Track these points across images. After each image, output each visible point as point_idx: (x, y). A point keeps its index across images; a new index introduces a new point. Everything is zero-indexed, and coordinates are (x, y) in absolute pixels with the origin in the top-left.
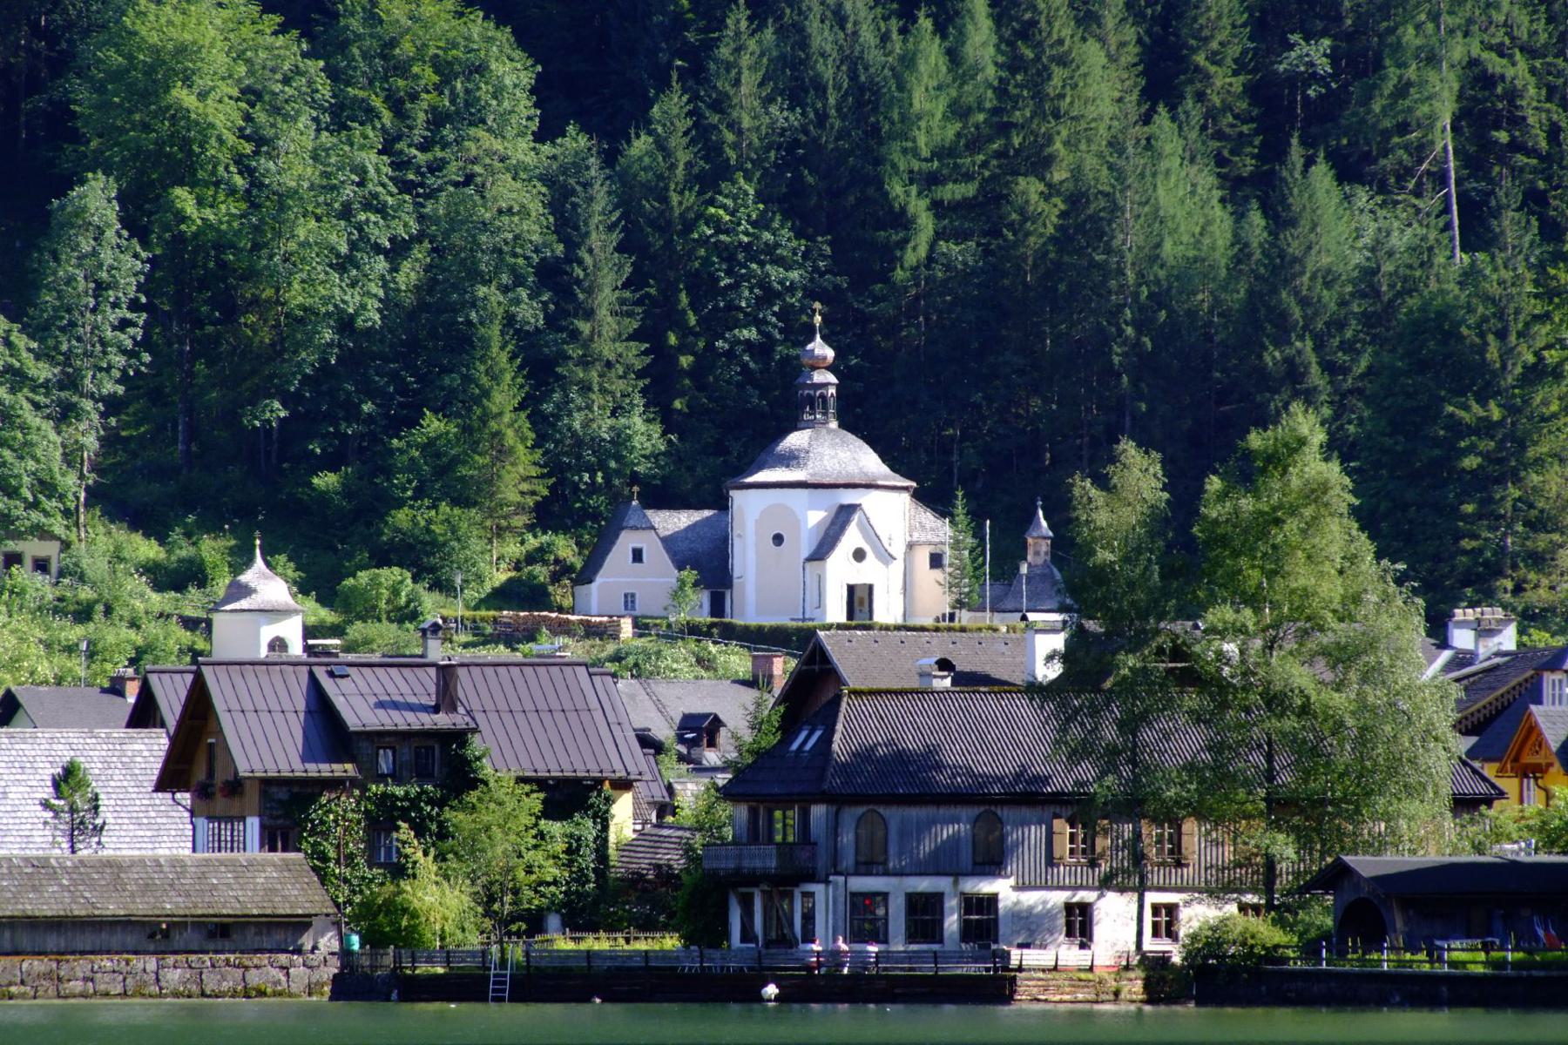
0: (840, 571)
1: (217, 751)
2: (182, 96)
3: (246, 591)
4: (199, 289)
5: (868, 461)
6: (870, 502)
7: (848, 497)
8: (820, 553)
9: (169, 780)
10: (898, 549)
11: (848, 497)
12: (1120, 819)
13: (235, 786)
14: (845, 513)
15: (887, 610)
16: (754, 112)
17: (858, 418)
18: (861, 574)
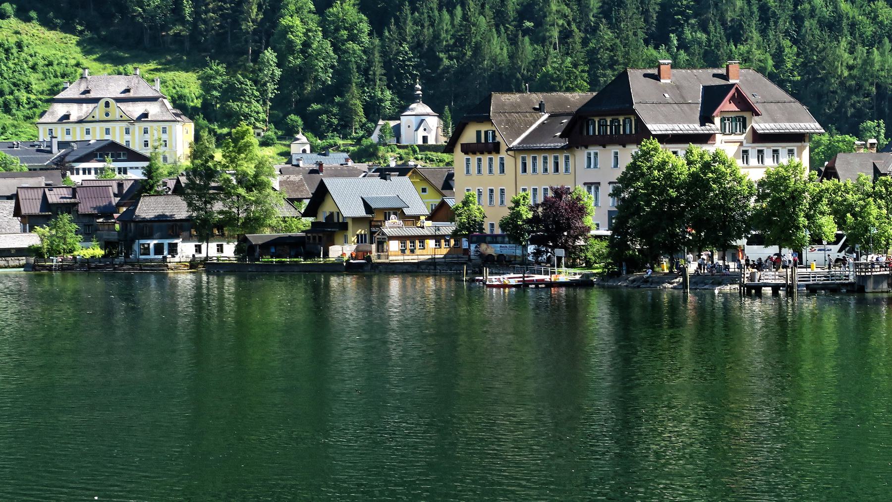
0: (421, 133)
3: (298, 139)
4: (293, 78)
5: (428, 110)
6: (428, 119)
12: (201, 228)
14: (423, 120)
15: (431, 141)
17: (427, 101)
18: (425, 134)
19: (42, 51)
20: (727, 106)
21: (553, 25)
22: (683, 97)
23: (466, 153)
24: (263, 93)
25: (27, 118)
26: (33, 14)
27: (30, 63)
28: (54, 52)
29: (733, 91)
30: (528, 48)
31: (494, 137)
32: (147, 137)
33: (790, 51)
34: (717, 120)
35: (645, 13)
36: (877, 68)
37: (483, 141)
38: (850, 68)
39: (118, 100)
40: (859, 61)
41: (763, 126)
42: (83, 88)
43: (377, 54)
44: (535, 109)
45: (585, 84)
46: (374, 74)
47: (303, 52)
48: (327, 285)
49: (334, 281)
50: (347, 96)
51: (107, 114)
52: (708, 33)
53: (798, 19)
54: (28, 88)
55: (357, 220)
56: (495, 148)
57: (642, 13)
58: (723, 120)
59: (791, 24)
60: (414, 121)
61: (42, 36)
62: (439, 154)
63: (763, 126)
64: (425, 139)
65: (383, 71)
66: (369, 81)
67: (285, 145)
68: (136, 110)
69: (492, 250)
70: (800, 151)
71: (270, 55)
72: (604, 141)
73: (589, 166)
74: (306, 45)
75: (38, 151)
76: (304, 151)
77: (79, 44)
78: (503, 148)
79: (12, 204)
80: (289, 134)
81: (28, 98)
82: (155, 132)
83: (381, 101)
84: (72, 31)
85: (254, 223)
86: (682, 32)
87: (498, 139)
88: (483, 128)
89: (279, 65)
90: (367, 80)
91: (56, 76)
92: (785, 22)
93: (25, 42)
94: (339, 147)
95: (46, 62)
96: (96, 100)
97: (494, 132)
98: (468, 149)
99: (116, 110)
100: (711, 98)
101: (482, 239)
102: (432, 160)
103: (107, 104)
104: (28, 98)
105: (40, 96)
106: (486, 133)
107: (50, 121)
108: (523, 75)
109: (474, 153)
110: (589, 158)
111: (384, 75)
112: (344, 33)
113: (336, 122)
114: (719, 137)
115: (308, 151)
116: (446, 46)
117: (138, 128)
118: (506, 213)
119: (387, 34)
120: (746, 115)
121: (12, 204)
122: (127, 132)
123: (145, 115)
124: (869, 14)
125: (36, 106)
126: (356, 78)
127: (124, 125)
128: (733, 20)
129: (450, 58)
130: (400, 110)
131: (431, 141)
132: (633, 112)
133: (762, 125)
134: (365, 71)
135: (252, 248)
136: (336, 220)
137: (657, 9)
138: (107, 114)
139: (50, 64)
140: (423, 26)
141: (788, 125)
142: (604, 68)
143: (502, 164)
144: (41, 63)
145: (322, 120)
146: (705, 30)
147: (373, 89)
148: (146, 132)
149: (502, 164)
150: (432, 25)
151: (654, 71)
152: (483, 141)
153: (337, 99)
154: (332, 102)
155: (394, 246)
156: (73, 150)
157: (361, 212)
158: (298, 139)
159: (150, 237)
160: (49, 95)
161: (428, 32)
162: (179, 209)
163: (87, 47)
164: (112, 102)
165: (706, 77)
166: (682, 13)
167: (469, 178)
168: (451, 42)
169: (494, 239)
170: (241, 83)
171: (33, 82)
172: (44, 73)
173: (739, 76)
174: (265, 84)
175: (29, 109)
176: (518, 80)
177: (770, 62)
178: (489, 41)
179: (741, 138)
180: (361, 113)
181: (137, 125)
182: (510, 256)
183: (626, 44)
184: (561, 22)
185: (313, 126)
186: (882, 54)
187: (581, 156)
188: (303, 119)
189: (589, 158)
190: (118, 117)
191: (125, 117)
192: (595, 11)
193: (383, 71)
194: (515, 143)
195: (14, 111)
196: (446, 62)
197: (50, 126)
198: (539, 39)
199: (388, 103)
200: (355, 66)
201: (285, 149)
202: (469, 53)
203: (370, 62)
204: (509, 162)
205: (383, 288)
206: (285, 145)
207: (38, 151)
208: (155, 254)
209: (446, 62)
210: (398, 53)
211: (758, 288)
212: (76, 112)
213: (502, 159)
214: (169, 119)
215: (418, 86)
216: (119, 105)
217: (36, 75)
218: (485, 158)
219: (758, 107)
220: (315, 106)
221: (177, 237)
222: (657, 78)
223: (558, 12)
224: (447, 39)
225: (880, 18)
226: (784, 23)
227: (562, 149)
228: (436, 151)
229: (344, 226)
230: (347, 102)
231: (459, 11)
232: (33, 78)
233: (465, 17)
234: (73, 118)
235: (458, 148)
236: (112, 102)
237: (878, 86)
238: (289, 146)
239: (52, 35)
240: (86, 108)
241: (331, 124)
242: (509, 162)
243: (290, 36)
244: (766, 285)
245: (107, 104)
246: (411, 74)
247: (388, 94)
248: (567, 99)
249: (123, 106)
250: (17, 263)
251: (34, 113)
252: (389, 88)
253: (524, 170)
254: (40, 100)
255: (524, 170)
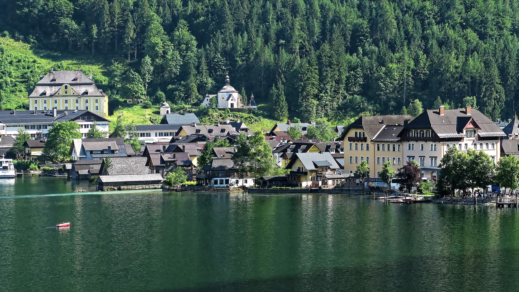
0: (230, 102)
1: (151, 163)
2: (157, 48)
3: (164, 105)
4: (159, 70)
5: (233, 89)
6: (234, 94)
7: (231, 93)
8: (228, 100)
9: (147, 165)
10: (236, 99)
11: (231, 93)
12: (242, 173)
13: (153, 166)
14: (231, 95)
15: (235, 106)
16: (220, 45)
17: (232, 84)
18: (233, 102)
19: (14, 54)
20: (469, 125)
21: (296, 42)
22: (449, 122)
23: (350, 141)
24: (144, 79)
25: (13, 92)
26: (6, 32)
27: (9, 60)
28: (20, 54)
29: (471, 119)
30: (285, 56)
31: (364, 135)
32: (87, 105)
33: (423, 57)
34: (464, 131)
35: (344, 35)
36: (472, 68)
37: (358, 136)
38: (456, 68)
39: (71, 84)
40: (461, 64)
41: (482, 133)
42: (51, 78)
43: (203, 59)
44: (380, 123)
45: (317, 76)
46: (202, 69)
47: (163, 57)
48: (301, 198)
49: (304, 196)
50: (188, 81)
51: (66, 93)
52: (379, 47)
53: (425, 38)
54: (10, 75)
55: (312, 171)
56: (365, 140)
57: (343, 35)
58: (466, 132)
59: (421, 41)
60: (226, 96)
61: (11, 44)
62: (241, 113)
63: (482, 133)
64: (232, 105)
65: (207, 68)
66: (199, 73)
67: (156, 108)
68: (82, 90)
69: (374, 184)
70: (497, 143)
71: (148, 59)
72: (417, 139)
73: (410, 149)
74: (165, 53)
75: (45, 115)
76: (168, 111)
77: (31, 48)
78: (369, 140)
79: (145, 159)
80: (157, 101)
81: (11, 81)
82: (92, 100)
83: (206, 84)
84: (28, 42)
85: (262, 170)
86: (364, 46)
87: (366, 136)
88: (358, 131)
89: (152, 65)
90: (199, 72)
91: (24, 68)
92: (418, 41)
93: (4, 49)
94: (186, 109)
95: (17, 60)
96: (61, 85)
97: (364, 133)
98: (350, 139)
99: (71, 90)
100: (461, 123)
101: (369, 180)
102: (237, 117)
103: (66, 87)
104: (11, 81)
105: (17, 80)
106: (360, 133)
107: (35, 96)
108: (282, 70)
109: (354, 141)
110: (410, 146)
111: (207, 70)
112: (184, 46)
113: (183, 95)
114: (465, 139)
115: (170, 112)
116: (240, 54)
117: (82, 100)
118: (381, 170)
119: (208, 47)
120: (476, 129)
121: (145, 159)
122: (77, 102)
123: (86, 93)
124: (463, 36)
125: (16, 85)
126: (194, 71)
127: (75, 98)
128: (391, 39)
129: (242, 61)
130: (216, 89)
131: (235, 106)
132: (431, 128)
133: (482, 134)
134: (197, 68)
135: (265, 182)
136: (301, 171)
137: (350, 33)
138: (66, 93)
139: (19, 61)
140: (227, 43)
141: (492, 133)
142: (326, 67)
143: (368, 147)
144: (15, 60)
145: (176, 94)
146: (377, 45)
147: (201, 77)
148: (87, 102)
149: (368, 147)
150: (232, 42)
151: (438, 111)
152: (358, 136)
153: (182, 82)
154: (180, 84)
155: (330, 182)
156: (65, 115)
157: (313, 168)
158: (164, 105)
159: (218, 177)
160: (22, 78)
161: (230, 46)
162: (230, 164)
163: (37, 50)
164: (68, 86)
165: (458, 113)
166: (364, 36)
167: (351, 151)
168: (243, 52)
169: (375, 180)
170: (133, 75)
171: (12, 71)
172: (17, 66)
173: (471, 112)
174: (145, 75)
175: (12, 87)
176: (279, 72)
177: (412, 63)
178: (264, 51)
179: (474, 138)
180: (196, 90)
181: (82, 98)
182: (382, 188)
183: (337, 54)
184: (300, 41)
185: (171, 98)
186: (473, 60)
187: (406, 145)
188: (165, 94)
189: (410, 146)
190: (72, 94)
191: (76, 94)
192: (317, 34)
193: (207, 68)
194: (374, 138)
195: (4, 88)
196: (240, 63)
197: (36, 99)
198: (291, 51)
199: (210, 85)
200: (193, 65)
201: (157, 110)
202: (252, 58)
203: (200, 63)
204: (371, 146)
205: (325, 201)
206: (156, 108)
207: (45, 115)
208: (220, 184)
209: (240, 63)
210: (214, 58)
211: (503, 205)
212: (49, 91)
213: (368, 144)
214: (97, 95)
215: (227, 76)
216: (72, 87)
217: (12, 67)
218: (359, 144)
219: (480, 125)
220: (170, 86)
221: (229, 177)
222: (439, 113)
223: (299, 35)
224: (240, 50)
225: (469, 38)
226: (418, 41)
227: (397, 141)
228: (239, 112)
229: (306, 174)
230: (187, 84)
231: (245, 35)
232: (12, 69)
233: (250, 39)
234: (48, 94)
235: (346, 139)
236: (68, 86)
237: (472, 78)
238: (159, 108)
239: (19, 44)
240: (54, 89)
241: (180, 96)
242: (371, 146)
243: (157, 48)
244: (506, 204)
245: (66, 87)
246: (222, 69)
247: (210, 80)
248: (392, 118)
249: (75, 88)
250: (153, 187)
251: (16, 89)
252: (210, 77)
253: (378, 150)
254: (18, 81)
255: (378, 150)
